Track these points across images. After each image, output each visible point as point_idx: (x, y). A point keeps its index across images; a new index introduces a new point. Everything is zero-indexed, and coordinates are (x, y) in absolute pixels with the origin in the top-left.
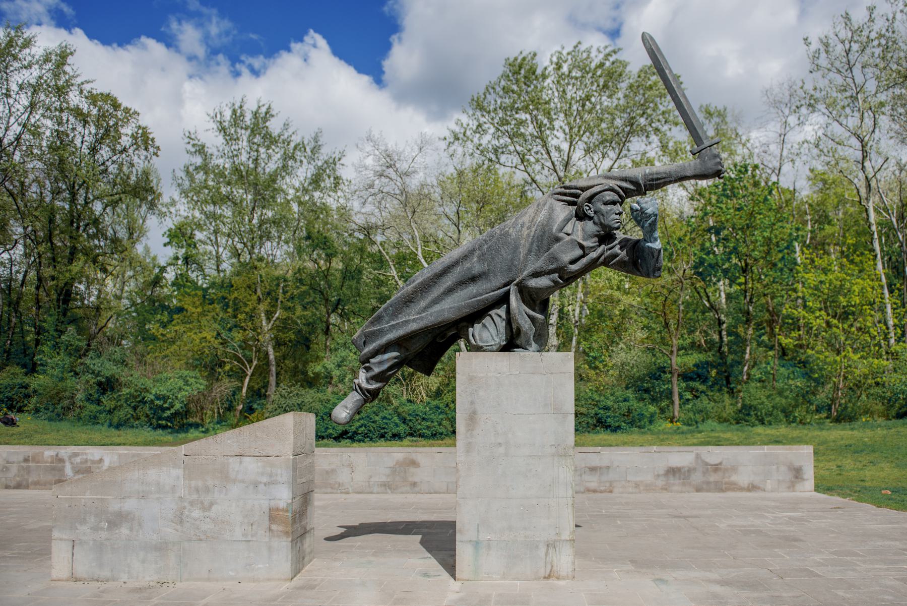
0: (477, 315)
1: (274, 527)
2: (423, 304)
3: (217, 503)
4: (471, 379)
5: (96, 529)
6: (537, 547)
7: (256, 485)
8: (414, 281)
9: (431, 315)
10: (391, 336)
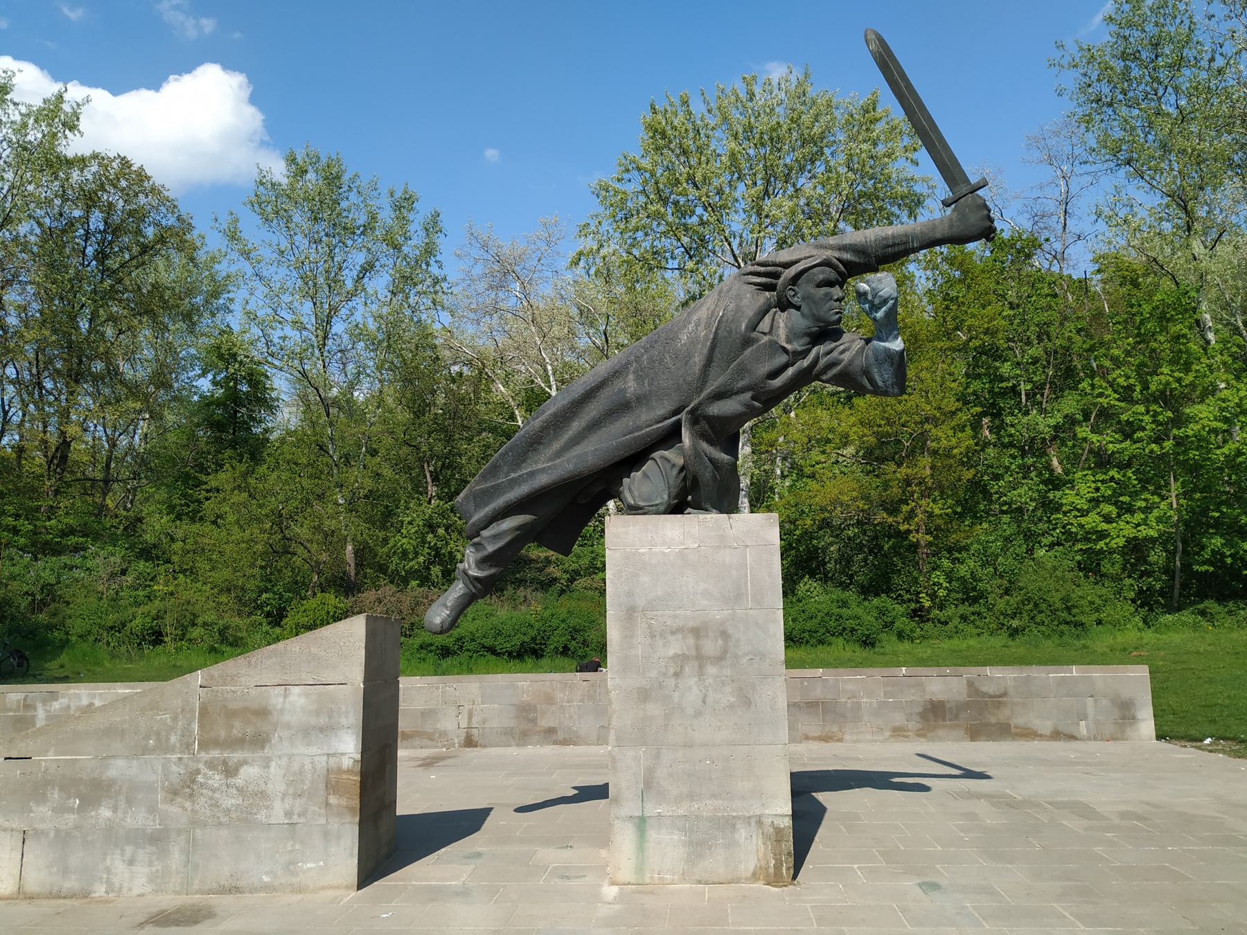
0: (634, 459)
2: (556, 446)
5: (61, 810)
8: (544, 412)
9: (568, 461)
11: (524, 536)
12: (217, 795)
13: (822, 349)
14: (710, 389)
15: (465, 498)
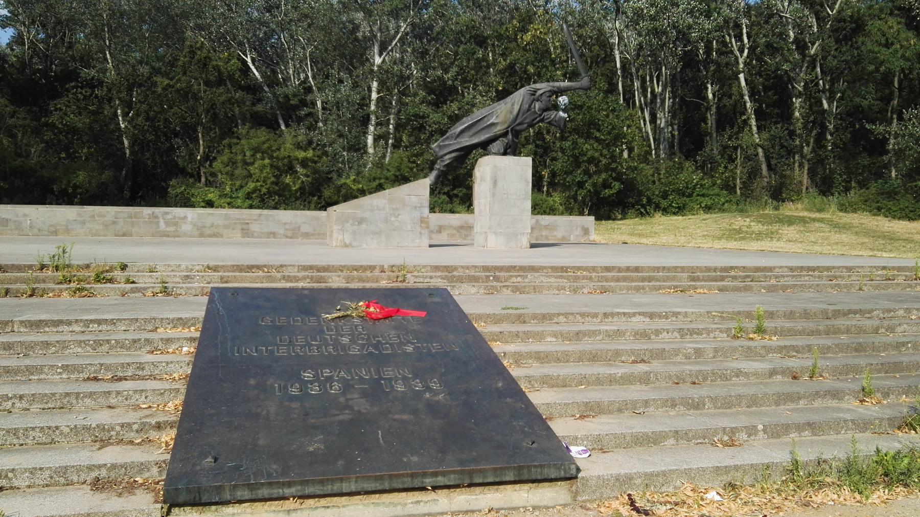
5: (352, 225)
7: (416, 208)
13: (546, 113)
14: (518, 122)
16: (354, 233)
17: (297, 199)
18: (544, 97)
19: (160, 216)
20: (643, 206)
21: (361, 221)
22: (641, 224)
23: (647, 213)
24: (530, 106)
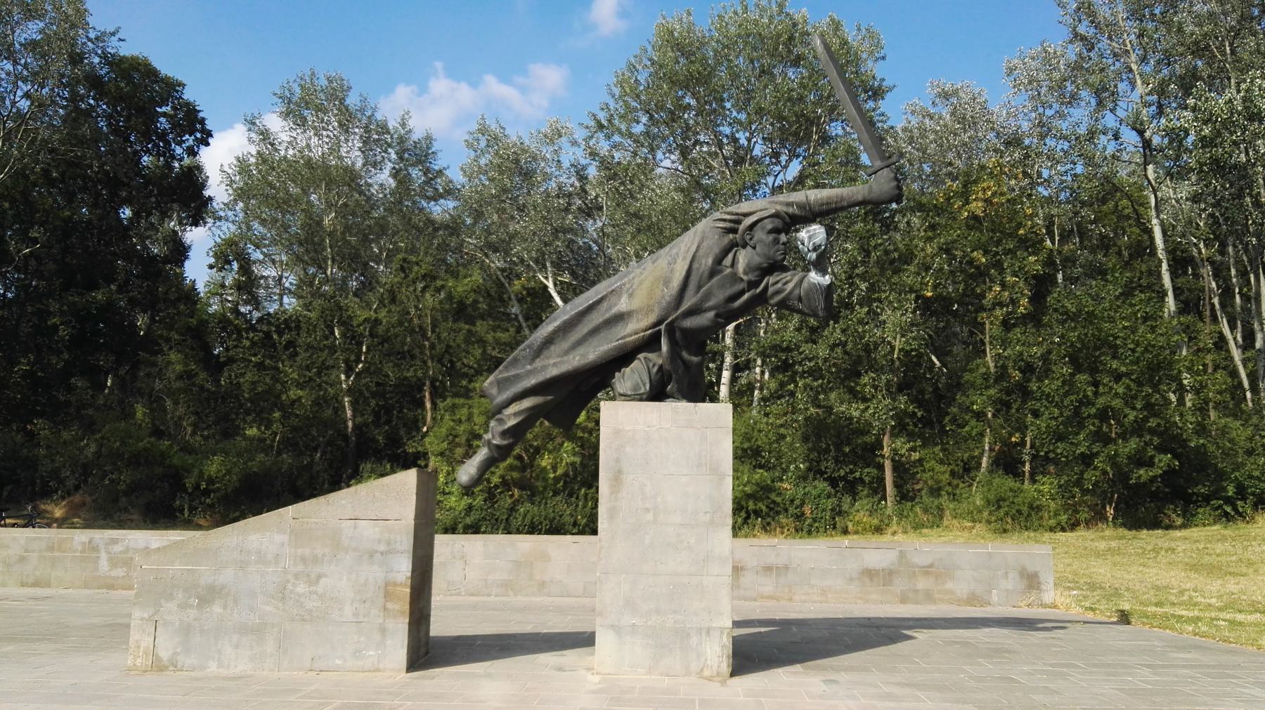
0: (623, 358)
1: (390, 605)
3: (325, 576)
4: (617, 432)
5: (183, 606)
6: (688, 635)
10: (532, 381)
11: (531, 417)
12: (302, 599)
13: (772, 279)
14: (685, 306)
15: (491, 383)
16: (186, 630)
17: (556, 493)
18: (759, 234)
19: (102, 547)
20: (1228, 501)
21: (209, 595)
22: (1223, 539)
23: (1240, 515)
24: (719, 261)
